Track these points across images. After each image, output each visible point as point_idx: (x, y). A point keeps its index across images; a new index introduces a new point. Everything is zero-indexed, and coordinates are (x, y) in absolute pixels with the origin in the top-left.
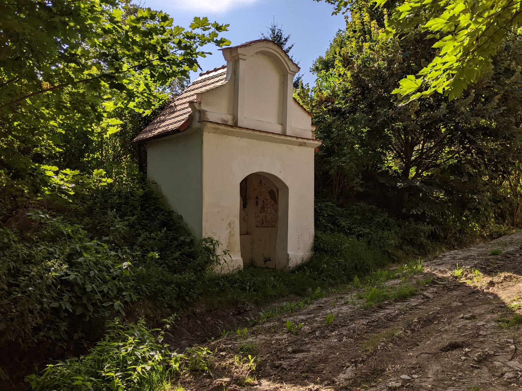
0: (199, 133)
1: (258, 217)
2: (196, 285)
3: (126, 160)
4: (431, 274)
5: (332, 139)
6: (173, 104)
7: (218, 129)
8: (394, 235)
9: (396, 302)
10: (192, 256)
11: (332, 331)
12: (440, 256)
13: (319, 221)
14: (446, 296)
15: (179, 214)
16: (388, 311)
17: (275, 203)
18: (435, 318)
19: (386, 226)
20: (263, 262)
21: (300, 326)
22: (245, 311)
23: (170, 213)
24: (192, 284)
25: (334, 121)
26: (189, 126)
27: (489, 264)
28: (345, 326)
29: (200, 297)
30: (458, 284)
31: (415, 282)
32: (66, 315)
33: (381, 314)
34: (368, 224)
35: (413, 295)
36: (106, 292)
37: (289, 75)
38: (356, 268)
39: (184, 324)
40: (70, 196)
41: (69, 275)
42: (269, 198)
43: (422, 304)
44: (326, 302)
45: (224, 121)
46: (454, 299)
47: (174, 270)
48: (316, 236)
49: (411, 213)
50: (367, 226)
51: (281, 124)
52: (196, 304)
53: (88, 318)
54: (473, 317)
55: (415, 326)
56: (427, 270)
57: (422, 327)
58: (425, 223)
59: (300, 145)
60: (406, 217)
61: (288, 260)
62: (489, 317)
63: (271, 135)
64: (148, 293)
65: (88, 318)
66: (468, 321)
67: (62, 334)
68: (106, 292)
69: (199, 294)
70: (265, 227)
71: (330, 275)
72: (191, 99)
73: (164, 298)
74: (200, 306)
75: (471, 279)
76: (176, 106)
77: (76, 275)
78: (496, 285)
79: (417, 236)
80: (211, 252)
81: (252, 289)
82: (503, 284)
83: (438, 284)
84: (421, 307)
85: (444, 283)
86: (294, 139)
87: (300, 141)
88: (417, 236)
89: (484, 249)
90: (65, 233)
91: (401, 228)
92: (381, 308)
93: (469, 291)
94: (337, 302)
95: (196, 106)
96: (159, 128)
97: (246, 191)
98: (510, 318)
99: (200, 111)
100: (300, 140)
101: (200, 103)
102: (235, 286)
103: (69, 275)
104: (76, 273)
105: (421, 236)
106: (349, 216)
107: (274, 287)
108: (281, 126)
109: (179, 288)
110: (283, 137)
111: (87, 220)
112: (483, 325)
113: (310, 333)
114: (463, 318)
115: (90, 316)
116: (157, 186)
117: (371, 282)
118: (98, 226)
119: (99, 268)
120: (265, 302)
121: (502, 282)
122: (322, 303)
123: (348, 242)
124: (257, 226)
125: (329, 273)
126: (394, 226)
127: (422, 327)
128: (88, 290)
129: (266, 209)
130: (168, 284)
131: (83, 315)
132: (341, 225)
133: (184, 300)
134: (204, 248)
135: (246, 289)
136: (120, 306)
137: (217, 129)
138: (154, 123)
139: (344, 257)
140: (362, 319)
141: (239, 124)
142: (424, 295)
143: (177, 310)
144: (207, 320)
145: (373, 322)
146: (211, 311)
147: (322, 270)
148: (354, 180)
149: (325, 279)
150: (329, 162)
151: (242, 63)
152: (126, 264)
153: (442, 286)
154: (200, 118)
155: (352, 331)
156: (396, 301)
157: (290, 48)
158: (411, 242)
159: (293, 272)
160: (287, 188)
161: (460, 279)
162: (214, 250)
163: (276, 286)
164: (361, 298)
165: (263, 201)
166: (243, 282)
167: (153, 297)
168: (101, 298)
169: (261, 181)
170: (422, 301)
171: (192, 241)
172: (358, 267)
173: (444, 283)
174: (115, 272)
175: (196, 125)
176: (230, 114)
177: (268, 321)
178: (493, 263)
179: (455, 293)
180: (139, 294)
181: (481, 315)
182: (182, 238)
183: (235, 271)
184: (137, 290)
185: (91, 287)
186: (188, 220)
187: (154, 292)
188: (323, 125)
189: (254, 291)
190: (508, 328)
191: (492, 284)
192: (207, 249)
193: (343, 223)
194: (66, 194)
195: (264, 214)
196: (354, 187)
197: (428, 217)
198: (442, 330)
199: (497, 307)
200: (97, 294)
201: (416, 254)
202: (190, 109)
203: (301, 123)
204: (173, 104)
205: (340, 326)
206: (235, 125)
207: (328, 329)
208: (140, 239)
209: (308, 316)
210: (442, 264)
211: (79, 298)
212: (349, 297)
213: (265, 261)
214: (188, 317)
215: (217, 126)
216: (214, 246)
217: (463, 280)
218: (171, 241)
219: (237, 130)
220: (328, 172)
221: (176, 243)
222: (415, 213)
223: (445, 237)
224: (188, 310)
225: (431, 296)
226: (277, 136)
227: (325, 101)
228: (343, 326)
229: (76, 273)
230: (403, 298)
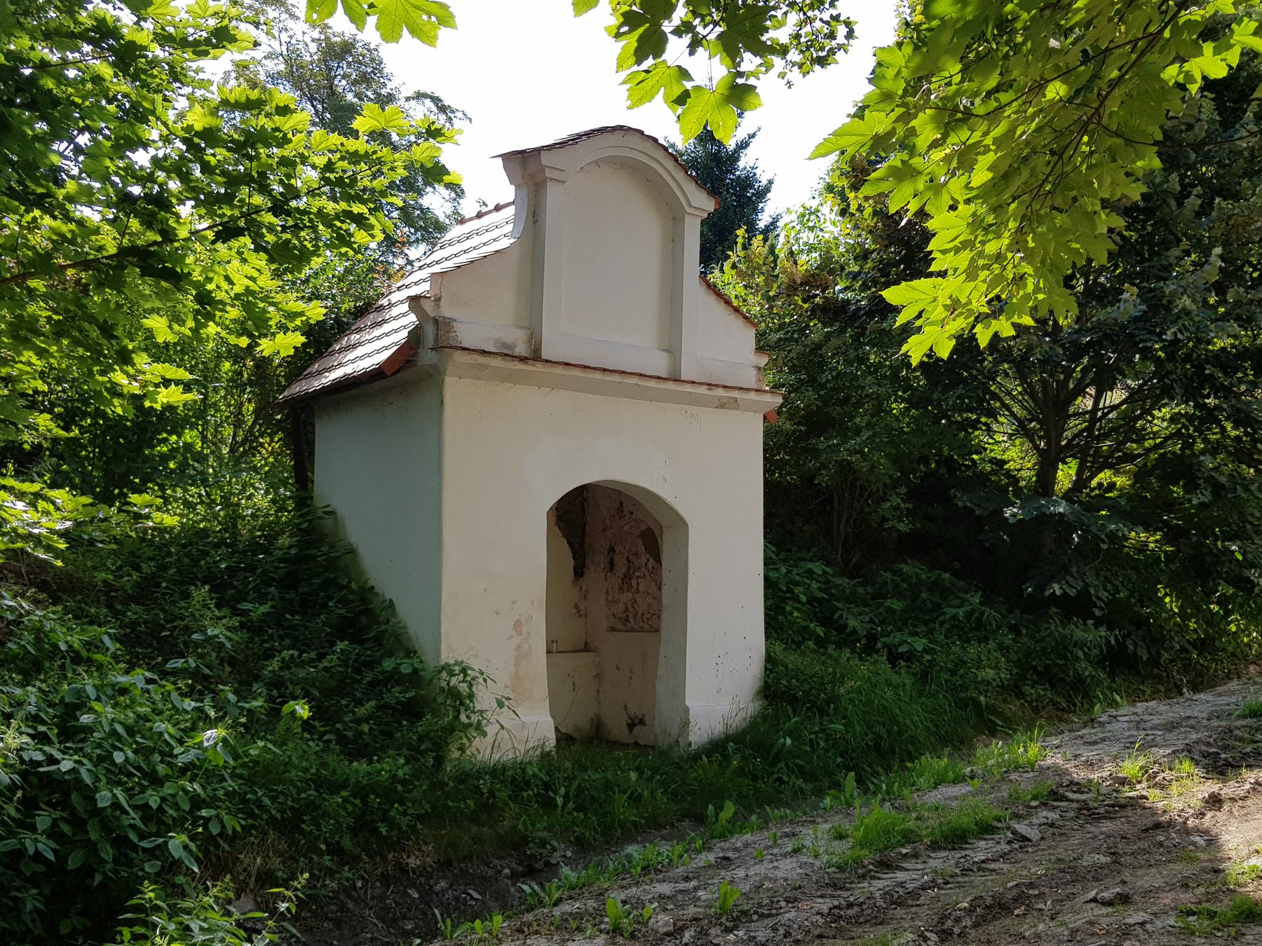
0: (434, 377)
1: (614, 602)
2: (411, 792)
3: (270, 447)
4: (1058, 771)
5: (822, 386)
6: (384, 302)
7: (486, 367)
8: (998, 654)
9: (934, 850)
10: (412, 711)
11: (728, 930)
12: (1104, 718)
13: (784, 613)
14: (1079, 835)
15: (388, 597)
16: (900, 876)
17: (656, 566)
18: (1020, 899)
19: (976, 629)
20: (626, 729)
21: (647, 912)
22: (547, 864)
23: (367, 592)
24: (400, 788)
25: (828, 336)
26: (408, 361)
27: (1231, 742)
28: (769, 916)
29: (419, 826)
30: (1122, 801)
31: (1005, 794)
32: (40, 868)
33: (878, 886)
34: (926, 624)
35: (986, 830)
36: (155, 807)
37: (687, 219)
38: (877, 747)
39: (373, 898)
40: (58, 554)
41: (57, 762)
42: (641, 549)
43: (1004, 856)
44: (746, 845)
45: (504, 345)
46: (1096, 844)
47: (355, 749)
48: (770, 659)
49: (1048, 593)
50: (921, 629)
51: (668, 351)
52: (411, 843)
53: (98, 878)
54: (1124, 899)
55: (958, 920)
56: (1053, 759)
57: (976, 925)
58: (1090, 622)
59: (722, 406)
60: (1037, 607)
61: (685, 724)
62: (1167, 901)
63: (635, 380)
64: (274, 812)
65: (98, 878)
66: (1104, 910)
67: (27, 919)
68: (155, 807)
69: (419, 818)
70: (633, 630)
71: (801, 768)
72: (414, 291)
73: (318, 827)
74: (419, 850)
75: (1163, 787)
76: (391, 305)
77: (76, 762)
78: (1226, 807)
79: (1064, 657)
80: (460, 700)
81: (571, 805)
82: (1248, 802)
83: (1068, 800)
84: (992, 866)
85: (1083, 797)
86: (703, 390)
87: (720, 394)
88: (1064, 657)
89: (1233, 700)
90: (63, 647)
91: (1018, 633)
92: (886, 865)
93: (1148, 822)
94: (775, 845)
95: (428, 306)
96: (340, 365)
97: (584, 531)
98: (1223, 906)
99: (436, 321)
100: (720, 392)
101: (438, 299)
102: (525, 794)
103: (57, 762)
104: (76, 757)
105: (1077, 659)
106: (871, 602)
107: (635, 799)
108: (665, 354)
109: (364, 801)
110: (670, 386)
111: (135, 612)
112: (1142, 924)
113: (667, 934)
114: (1094, 900)
115: (104, 874)
116: (336, 519)
117: (888, 792)
118: (165, 629)
119: (136, 742)
120: (607, 842)
121: (1244, 798)
122: (736, 850)
123: (858, 675)
124: (613, 629)
125: (798, 761)
126: (999, 627)
127: (976, 925)
128: (100, 805)
129: (634, 582)
130: (334, 788)
131: (87, 871)
132: (846, 626)
133: (376, 831)
134: (442, 690)
135: (556, 805)
136: (186, 847)
137: (482, 367)
138: (332, 354)
139: (845, 717)
140: (822, 896)
141: (544, 356)
142: (1014, 833)
143: (353, 861)
144: (438, 888)
145: (850, 905)
146: (449, 863)
147: (778, 753)
148: (885, 499)
149: (785, 778)
150: (815, 453)
151: (552, 191)
152: (211, 735)
153: (1075, 805)
154: (436, 340)
155: (782, 931)
156: (935, 846)
157: (753, 136)
158: (1047, 677)
159: (697, 756)
160: (684, 524)
161: (1132, 786)
162: (471, 696)
163: (641, 795)
164: (840, 837)
165: (628, 560)
166: (547, 786)
167: (288, 826)
168: (138, 823)
169: (621, 503)
170: (1007, 848)
171: (416, 672)
172: (885, 745)
173: (1083, 797)
174: (184, 757)
175: (427, 357)
176: (522, 328)
177: (571, 898)
178: (1241, 739)
179: (1107, 826)
180: (251, 815)
181: (1147, 893)
182: (388, 664)
183: (531, 752)
184: (240, 803)
185: (109, 795)
186: (409, 615)
187: (292, 808)
188: (796, 350)
189: (577, 809)
190: (1208, 935)
191: (1215, 802)
192: (454, 694)
193: (852, 623)
194: (49, 548)
195: (630, 595)
196: (884, 519)
197: (1099, 603)
198: (1027, 934)
199: (1203, 870)
200: (127, 813)
201: (1063, 710)
202: (412, 318)
203: (726, 346)
204: (384, 302)
205: (755, 917)
206: (535, 356)
207: (721, 924)
208: (275, 664)
209: (682, 886)
210: (1103, 740)
211: (79, 824)
212: (808, 835)
213: (631, 726)
214: (385, 879)
215: (481, 359)
216: (471, 686)
217: (1141, 789)
218: (358, 671)
219: (539, 367)
220: (814, 476)
221: (369, 677)
222: (1058, 592)
223: (1154, 661)
224: (384, 859)
225: (1033, 834)
226: (652, 384)
227: (802, 284)
228: (762, 916)
229: (76, 757)
230: (956, 838)
